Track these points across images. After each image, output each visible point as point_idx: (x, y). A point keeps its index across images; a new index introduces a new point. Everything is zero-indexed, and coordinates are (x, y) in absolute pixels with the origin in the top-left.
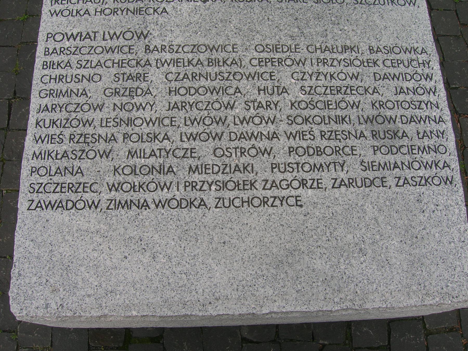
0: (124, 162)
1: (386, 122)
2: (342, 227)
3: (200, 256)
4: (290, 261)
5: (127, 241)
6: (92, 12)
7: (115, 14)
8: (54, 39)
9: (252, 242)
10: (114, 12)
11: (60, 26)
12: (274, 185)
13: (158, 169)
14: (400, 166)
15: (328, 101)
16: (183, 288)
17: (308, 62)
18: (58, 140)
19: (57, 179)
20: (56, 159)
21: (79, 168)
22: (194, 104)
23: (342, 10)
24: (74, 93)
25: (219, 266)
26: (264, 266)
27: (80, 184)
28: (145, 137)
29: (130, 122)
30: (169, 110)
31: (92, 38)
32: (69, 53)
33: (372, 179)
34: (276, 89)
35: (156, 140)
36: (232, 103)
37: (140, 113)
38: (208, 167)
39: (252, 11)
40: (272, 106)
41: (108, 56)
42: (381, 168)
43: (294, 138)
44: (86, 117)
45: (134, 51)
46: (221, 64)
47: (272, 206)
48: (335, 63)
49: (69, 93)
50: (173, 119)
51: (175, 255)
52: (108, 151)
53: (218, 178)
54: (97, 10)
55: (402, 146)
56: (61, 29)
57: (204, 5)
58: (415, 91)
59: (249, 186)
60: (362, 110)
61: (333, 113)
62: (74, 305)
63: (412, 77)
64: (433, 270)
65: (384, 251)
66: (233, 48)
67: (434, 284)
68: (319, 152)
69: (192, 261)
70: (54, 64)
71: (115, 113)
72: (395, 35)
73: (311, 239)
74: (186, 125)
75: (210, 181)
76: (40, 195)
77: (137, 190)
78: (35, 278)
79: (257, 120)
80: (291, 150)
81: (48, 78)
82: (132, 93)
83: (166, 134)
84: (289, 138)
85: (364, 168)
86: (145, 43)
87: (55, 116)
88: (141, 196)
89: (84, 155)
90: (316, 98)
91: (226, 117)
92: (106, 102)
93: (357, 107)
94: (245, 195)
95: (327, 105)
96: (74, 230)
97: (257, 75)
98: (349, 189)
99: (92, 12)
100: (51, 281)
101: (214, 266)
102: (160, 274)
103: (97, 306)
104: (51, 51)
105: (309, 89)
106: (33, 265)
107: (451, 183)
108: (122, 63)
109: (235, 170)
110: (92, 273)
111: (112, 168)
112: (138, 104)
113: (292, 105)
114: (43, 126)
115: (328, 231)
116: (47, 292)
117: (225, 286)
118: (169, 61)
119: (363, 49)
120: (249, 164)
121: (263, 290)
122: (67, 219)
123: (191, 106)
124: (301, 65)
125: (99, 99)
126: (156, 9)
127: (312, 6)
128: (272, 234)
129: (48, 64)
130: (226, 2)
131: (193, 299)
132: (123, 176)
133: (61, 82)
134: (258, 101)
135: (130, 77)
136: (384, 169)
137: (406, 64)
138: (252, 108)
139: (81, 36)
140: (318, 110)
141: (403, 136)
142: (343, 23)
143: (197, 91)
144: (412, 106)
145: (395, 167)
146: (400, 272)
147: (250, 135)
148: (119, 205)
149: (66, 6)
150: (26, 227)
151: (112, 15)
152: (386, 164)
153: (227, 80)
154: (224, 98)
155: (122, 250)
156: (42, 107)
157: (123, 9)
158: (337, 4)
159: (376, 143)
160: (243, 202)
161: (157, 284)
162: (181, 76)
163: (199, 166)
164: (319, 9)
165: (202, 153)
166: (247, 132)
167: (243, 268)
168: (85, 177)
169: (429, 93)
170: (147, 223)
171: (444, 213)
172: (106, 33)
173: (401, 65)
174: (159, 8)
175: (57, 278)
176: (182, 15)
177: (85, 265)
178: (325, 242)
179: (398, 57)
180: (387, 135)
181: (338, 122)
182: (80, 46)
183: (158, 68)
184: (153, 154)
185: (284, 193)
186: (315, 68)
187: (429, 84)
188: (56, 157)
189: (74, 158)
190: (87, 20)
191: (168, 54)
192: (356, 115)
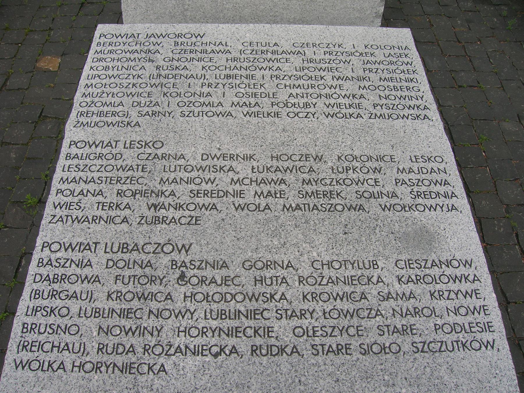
6: (69, 367)
7: (98, 371)
10: (97, 368)
11: (25, 385)
23: (398, 364)
39: (278, 369)
54: (75, 364)
56: (27, 389)
57: (215, 361)
99: (69, 367)
126: (151, 365)
127: (358, 359)
130: (244, 357)
142: (400, 383)
149: (36, 354)
151: (94, 372)
157: (108, 363)
158: (391, 354)
164: (367, 364)
174: (155, 364)
190: (60, 378)
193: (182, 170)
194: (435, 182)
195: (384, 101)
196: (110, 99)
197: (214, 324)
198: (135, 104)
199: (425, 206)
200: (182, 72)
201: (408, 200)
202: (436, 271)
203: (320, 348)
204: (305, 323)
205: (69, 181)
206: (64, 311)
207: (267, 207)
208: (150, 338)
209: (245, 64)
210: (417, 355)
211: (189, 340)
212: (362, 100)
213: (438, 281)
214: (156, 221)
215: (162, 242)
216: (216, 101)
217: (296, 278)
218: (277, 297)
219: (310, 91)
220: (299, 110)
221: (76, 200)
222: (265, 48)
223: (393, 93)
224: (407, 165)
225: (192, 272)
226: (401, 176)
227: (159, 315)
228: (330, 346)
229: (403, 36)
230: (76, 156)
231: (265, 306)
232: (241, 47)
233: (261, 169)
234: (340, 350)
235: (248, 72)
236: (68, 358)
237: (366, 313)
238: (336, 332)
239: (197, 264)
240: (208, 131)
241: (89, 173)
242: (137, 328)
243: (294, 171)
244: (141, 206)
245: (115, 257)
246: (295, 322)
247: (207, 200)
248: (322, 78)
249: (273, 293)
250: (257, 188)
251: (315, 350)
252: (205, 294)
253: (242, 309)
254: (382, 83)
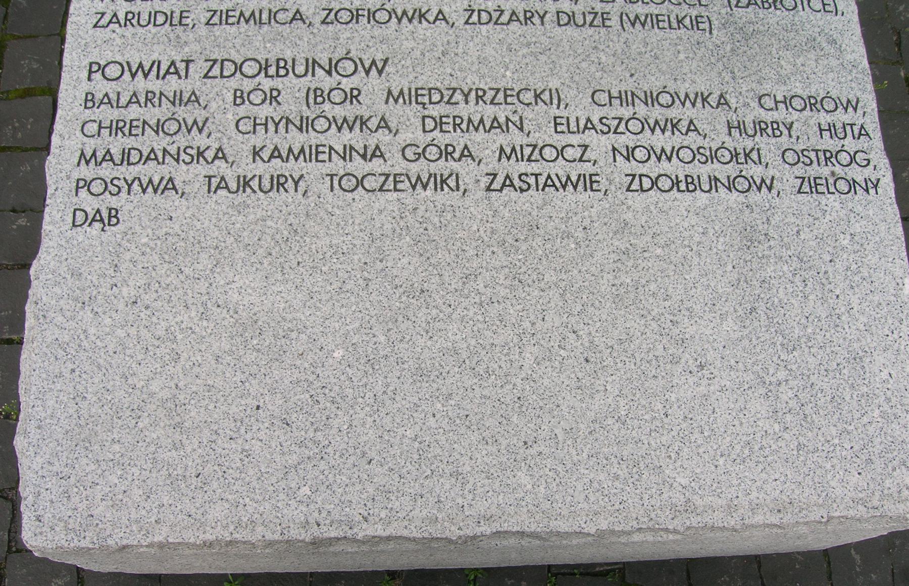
8: (89, 190)
24: (336, 152)
31: (183, 73)
42: (291, 157)
181: (304, 128)
194: (658, 153)
203: (532, 180)
205: (99, 160)
213: (832, 189)
234: (529, 19)
252: (263, 63)
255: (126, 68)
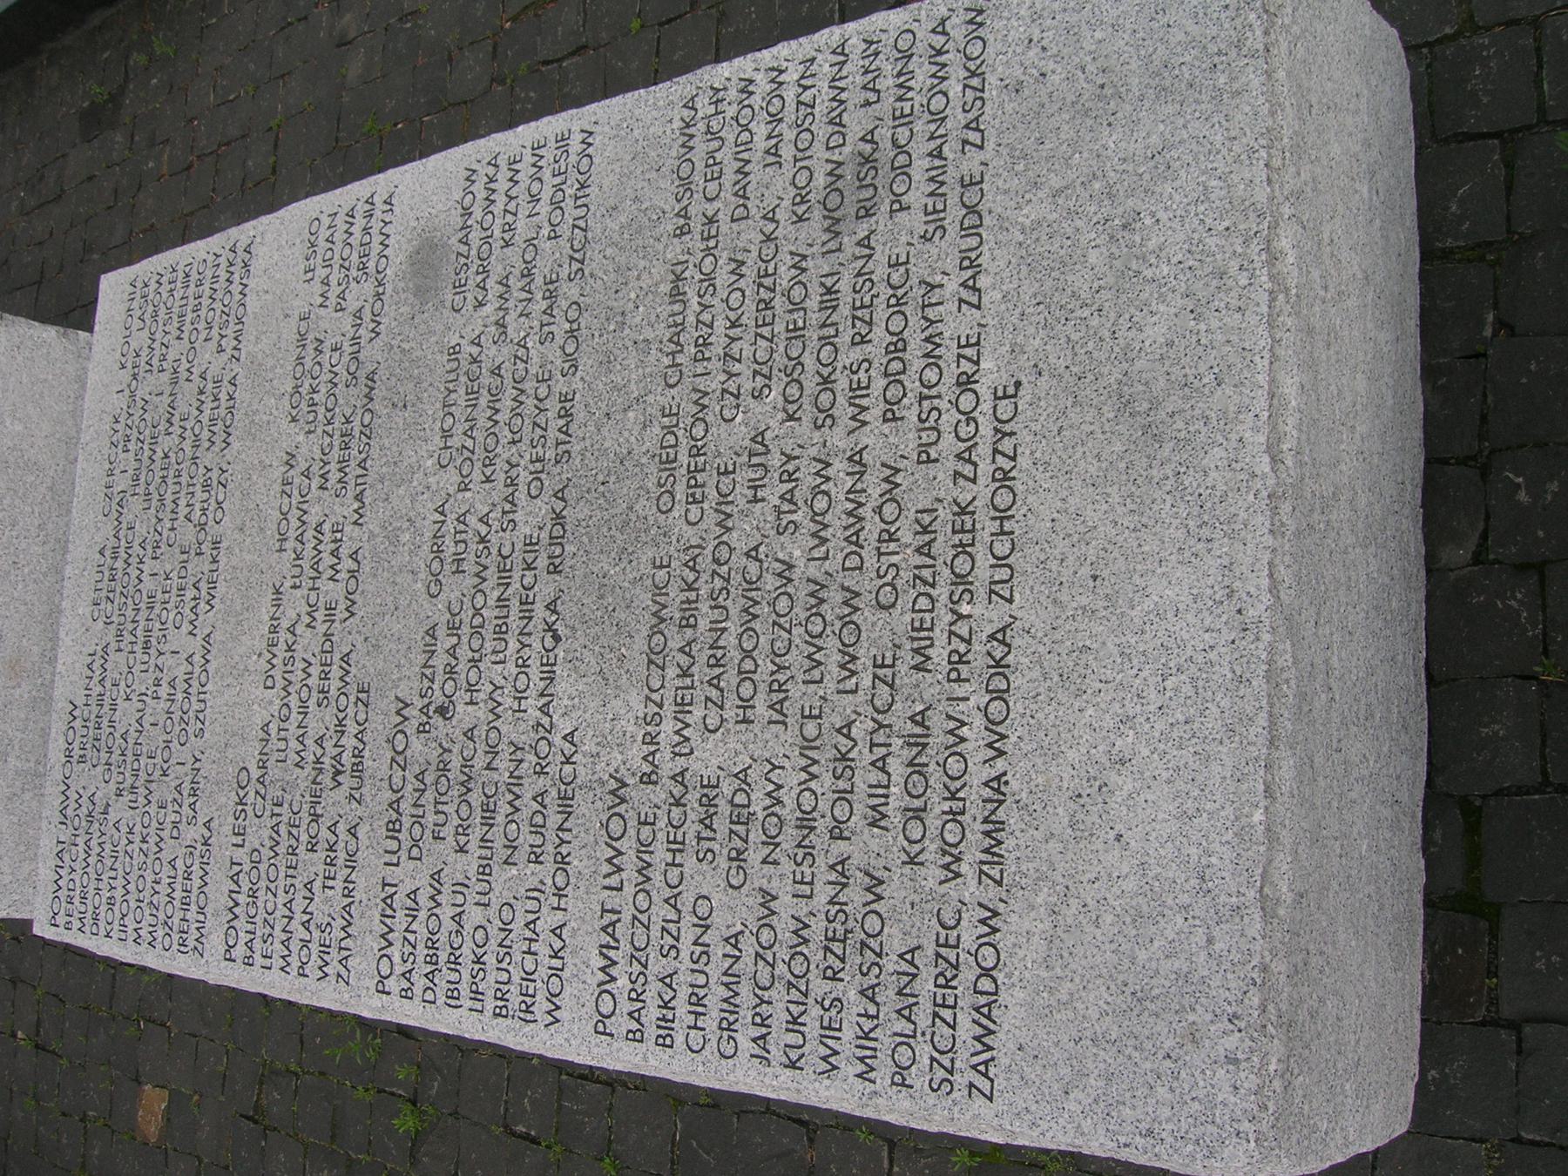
0: (894, 839)
1: (839, 184)
2: (1070, 278)
3: (1123, 639)
4: (1146, 405)
5: (1079, 833)
9: (1097, 506)
10: (562, 862)
12: (966, 455)
13: (915, 750)
14: (939, 141)
15: (788, 331)
16: (1201, 683)
17: (701, 383)
18: (834, 1012)
19: (923, 1019)
20: (877, 1017)
21: (901, 956)
22: (777, 660)
25: (1149, 590)
26: (1154, 472)
27: (938, 955)
28: (842, 784)
29: (806, 823)
30: (785, 724)
31: (615, 917)
32: (642, 979)
33: (964, 211)
34: (755, 460)
35: (850, 756)
36: (779, 567)
37: (788, 798)
38: (917, 624)
40: (790, 467)
41: (657, 877)
43: (864, 409)
44: (786, 937)
45: (650, 812)
46: (692, 596)
47: (1013, 459)
48: (706, 317)
49: (731, 980)
50: (807, 713)
51: (1117, 705)
52: (867, 879)
53: (944, 598)
55: (894, 142)
58: (776, 119)
59: (967, 518)
60: (811, 245)
61: (815, 318)
62: (1232, 985)
63: (745, 128)
64: (1181, 37)
65: (1130, 168)
66: (662, 567)
67: (1214, 31)
68: (897, 347)
69: (1135, 662)
70: (664, 1019)
71: (783, 860)
72: (654, 175)
73: (1095, 354)
74: (821, 681)
75: (949, 617)
76: (958, 1064)
77: (961, 804)
78: (1159, 1089)
79: (821, 504)
80: (889, 415)
81: (693, 1033)
82: (741, 817)
83: (839, 731)
84: (864, 423)
85: (939, 234)
86: (635, 785)
87: (779, 1017)
88: (975, 794)
89: (873, 943)
90: (780, 359)
91: (809, 580)
92: (757, 885)
93: (804, 257)
94: (987, 526)
95: (795, 333)
96: (1045, 974)
97: (723, 507)
98: (985, 266)
100: (1169, 1043)
101: (1148, 604)
102: (1162, 746)
103: (1237, 920)
104: (635, 1026)
105: (758, 378)
106: (1128, 1095)
107: (980, 12)
108: (675, 842)
109: (928, 555)
110: (1154, 929)
111: (907, 869)
112: (768, 802)
113: (791, 418)
114: (800, 1051)
115: (1078, 313)
116: (1196, 1058)
117: (1200, 574)
118: (680, 725)
119: (679, 250)
120: (917, 521)
121: (1213, 474)
122: (1020, 995)
123: (780, 668)
124: (705, 401)
125: (750, 901)
128: (1079, 455)
129: (661, 1032)
131: (1228, 658)
132: (927, 842)
133: (705, 1001)
134: (777, 502)
135: (706, 822)
136: (942, 183)
137: (716, 144)
138: (794, 517)
139: (608, 947)
140: (806, 354)
141: (872, 141)
143: (748, 654)
144: (806, 125)
145: (940, 156)
146: (1181, 121)
147: (852, 520)
148: (994, 854)
150: (1033, 1108)
152: (932, 179)
153: (728, 581)
154: (768, 587)
155: (1100, 846)
156: (758, 1051)
159: (885, 207)
160: (1003, 533)
161: (1187, 755)
162: (714, 693)
163: (916, 645)
165: (886, 641)
166: (846, 528)
167: (1158, 528)
168: (924, 941)
169: (781, 84)
170: (1040, 780)
171: (1049, 21)
172: (607, 882)
173: (719, 156)
175: (1161, 1027)
176: (581, 694)
177: (1132, 950)
178: (1103, 319)
179: (700, 166)
180: (868, 180)
182: (629, 949)
183: (692, 752)
184: (880, 764)
185: (986, 429)
186: (715, 365)
187: (762, 84)
188: (873, 1017)
189: (877, 970)
191: (662, 727)
192: (820, 261)
193: (286, 725)
195: (215, 332)
196: (163, 889)
197: (513, 645)
198: (175, 834)
199: (381, 256)
200: (131, 741)
201: (369, 287)
202: (475, 236)
204: (524, 477)
206: (480, 935)
207: (354, 556)
208: (525, 765)
209: (130, 613)
210: (586, 273)
211: (533, 692)
212: (209, 377)
214: (358, 769)
215: (389, 754)
216: (185, 667)
217: (460, 496)
218: (484, 530)
219: (184, 479)
220: (212, 501)
221: (316, 934)
222: (107, 574)
223: (203, 313)
224: (317, 288)
225: (438, 693)
226: (333, 300)
227: (493, 751)
228: (560, 430)
229: (113, 287)
230: (249, 945)
231: (494, 551)
232: (100, 624)
233: (297, 571)
235: (143, 606)
236: (548, 920)
237: (521, 365)
238: (541, 420)
239: (426, 683)
240: (230, 680)
241: (278, 914)
242: (510, 791)
243: (305, 506)
244: (334, 801)
245: (406, 844)
246: (521, 496)
247: (336, 672)
248: (166, 456)
249: (477, 539)
250: (325, 576)
251: (563, 457)
253: (496, 594)
254: (185, 336)
255: (985, 940)
